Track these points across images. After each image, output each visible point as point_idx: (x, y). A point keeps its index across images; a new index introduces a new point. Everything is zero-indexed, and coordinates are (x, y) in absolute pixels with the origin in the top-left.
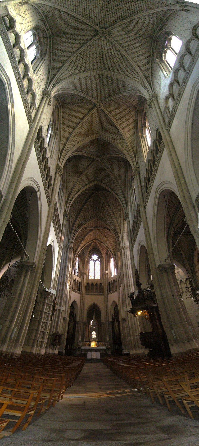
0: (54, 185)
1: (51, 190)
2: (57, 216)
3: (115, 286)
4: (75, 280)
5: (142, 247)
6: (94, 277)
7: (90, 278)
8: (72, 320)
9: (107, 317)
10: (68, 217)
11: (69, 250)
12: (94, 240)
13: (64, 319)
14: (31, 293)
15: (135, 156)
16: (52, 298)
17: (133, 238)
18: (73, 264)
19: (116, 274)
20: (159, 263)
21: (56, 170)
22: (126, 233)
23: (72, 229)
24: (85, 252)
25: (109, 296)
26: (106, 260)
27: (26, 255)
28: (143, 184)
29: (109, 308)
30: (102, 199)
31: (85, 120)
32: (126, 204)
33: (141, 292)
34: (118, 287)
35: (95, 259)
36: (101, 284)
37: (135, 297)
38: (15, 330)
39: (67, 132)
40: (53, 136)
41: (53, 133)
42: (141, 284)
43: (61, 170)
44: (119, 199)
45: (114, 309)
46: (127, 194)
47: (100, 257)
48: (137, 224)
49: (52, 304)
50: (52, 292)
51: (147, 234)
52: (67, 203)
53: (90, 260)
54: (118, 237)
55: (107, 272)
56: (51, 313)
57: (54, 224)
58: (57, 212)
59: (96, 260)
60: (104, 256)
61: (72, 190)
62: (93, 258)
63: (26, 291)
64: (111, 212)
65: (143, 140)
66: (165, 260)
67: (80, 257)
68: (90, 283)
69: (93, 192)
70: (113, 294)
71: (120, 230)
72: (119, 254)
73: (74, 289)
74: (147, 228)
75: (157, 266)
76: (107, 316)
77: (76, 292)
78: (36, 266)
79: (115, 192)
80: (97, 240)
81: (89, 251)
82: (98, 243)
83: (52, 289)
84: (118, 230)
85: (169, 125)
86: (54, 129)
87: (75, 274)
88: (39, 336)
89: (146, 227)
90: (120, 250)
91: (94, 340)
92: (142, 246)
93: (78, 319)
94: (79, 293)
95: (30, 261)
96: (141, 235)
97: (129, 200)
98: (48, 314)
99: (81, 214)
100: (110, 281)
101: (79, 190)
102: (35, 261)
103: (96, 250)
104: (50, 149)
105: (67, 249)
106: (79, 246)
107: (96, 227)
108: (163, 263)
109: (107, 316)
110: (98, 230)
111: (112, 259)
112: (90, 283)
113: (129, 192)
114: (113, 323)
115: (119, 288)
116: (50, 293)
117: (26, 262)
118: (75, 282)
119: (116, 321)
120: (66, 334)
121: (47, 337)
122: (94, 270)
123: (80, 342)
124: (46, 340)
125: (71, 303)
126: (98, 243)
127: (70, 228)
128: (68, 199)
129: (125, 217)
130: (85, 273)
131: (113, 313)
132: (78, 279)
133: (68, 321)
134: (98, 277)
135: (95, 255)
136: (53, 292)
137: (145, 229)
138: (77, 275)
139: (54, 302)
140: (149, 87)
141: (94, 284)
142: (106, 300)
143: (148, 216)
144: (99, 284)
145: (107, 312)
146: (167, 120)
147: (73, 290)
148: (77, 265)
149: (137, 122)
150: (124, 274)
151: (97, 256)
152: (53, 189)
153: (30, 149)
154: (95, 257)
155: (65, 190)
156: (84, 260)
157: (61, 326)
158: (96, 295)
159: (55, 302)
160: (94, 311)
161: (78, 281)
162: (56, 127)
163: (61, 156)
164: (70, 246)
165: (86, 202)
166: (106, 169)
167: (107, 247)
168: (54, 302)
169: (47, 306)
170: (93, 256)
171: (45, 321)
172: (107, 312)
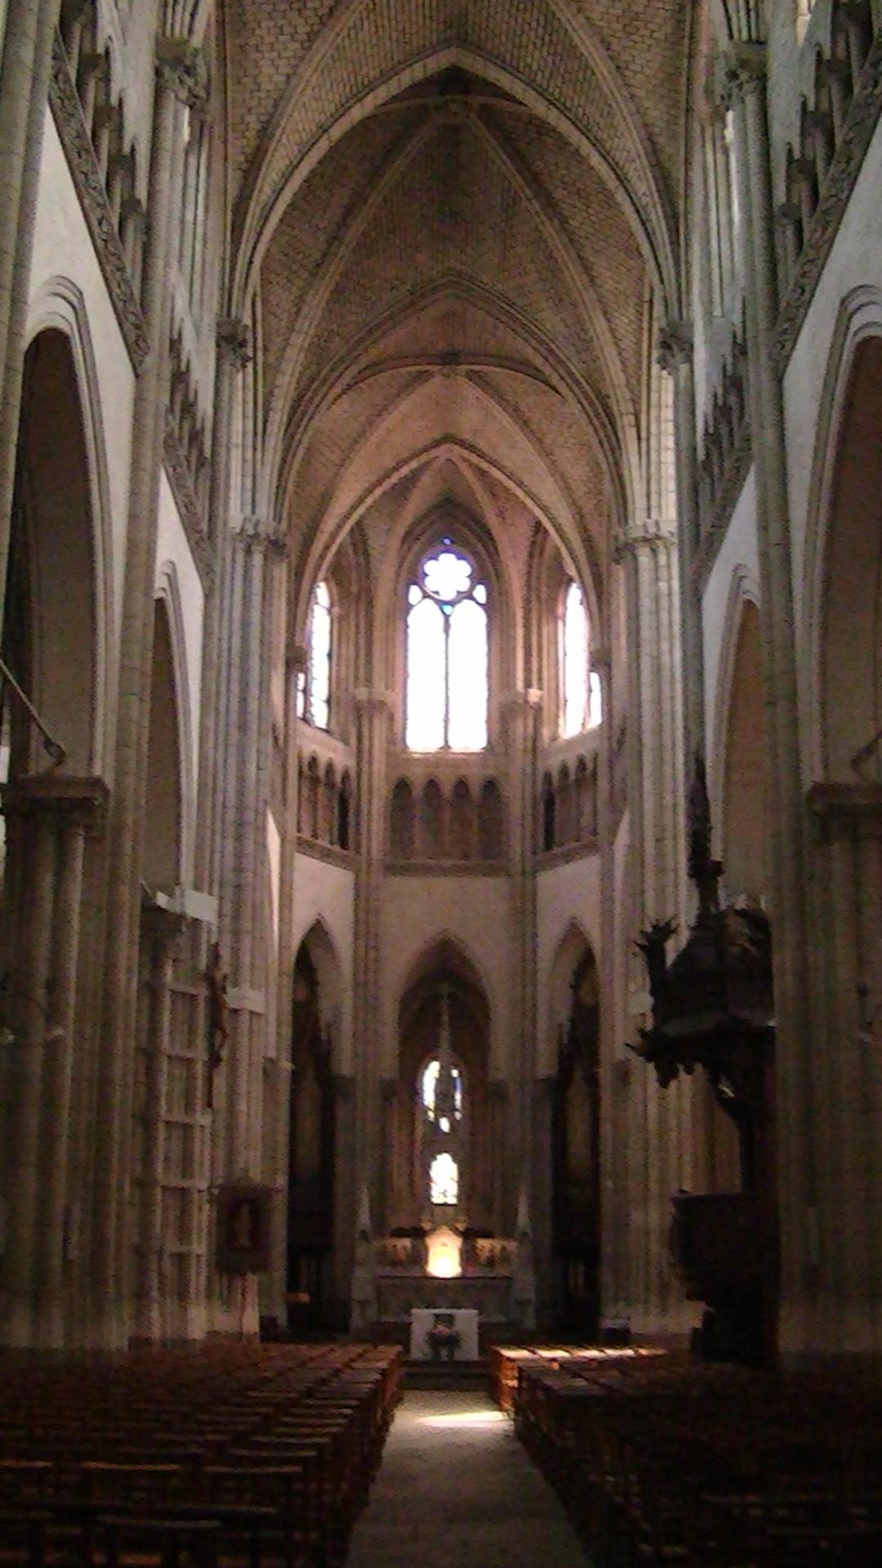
0: (151, 196)
1: (208, 484)
2: (96, 64)
3: (587, 808)
4: (314, 761)
8: (311, 1075)
9: (525, 1042)
12: (437, 444)
13: (269, 1071)
14: (109, 967)
16: (195, 949)
17: (789, 269)
18: (290, 645)
19: (596, 720)
20: (818, 775)
21: (158, 72)
22: (669, 414)
24: (375, 542)
25: (546, 879)
26: (527, 601)
27: (48, 743)
28: (780, 195)
29: (542, 977)
30: (500, 160)
32: (675, 243)
33: (709, 923)
36: (490, 786)
37: (673, 949)
38: (76, 1217)
42: (718, 869)
43: (189, 71)
44: (620, 196)
45: (575, 987)
46: (688, 162)
47: (487, 572)
49: (203, 992)
50: (192, 911)
52: (236, 242)
53: (415, 593)
54: (614, 449)
55: (534, 695)
56: (200, 1054)
57: (177, 485)
60: (515, 571)
61: (265, 132)
62: (430, 584)
64: (564, 255)
65: (720, 158)
66: (855, 763)
67: (337, 577)
69: (425, 108)
70: (567, 870)
71: (635, 402)
72: (621, 573)
73: (306, 835)
74: (774, 513)
75: (807, 786)
76: (524, 1029)
77: (325, 855)
78: (106, 791)
79: (596, 143)
80: (462, 443)
81: (401, 529)
82: (468, 473)
83: (190, 893)
84: (621, 404)
87: (306, 719)
88: (164, 1226)
89: (773, 505)
90: (624, 551)
91: (443, 1216)
93: (345, 1064)
94: (343, 863)
95: (74, 768)
96: (741, 540)
97: (697, 215)
98: (189, 1062)
100: (554, 764)
101: (324, 130)
102: (97, 771)
103: (457, 522)
105: (248, 552)
106: (326, 499)
107: (450, 359)
108: (844, 775)
110: (473, 376)
111: (575, 594)
113: (697, 159)
114: (559, 1086)
115: (613, 830)
116: (182, 917)
117: (47, 779)
118: (315, 780)
119: (578, 1075)
121: (203, 1216)
122: (445, 690)
123: (364, 1236)
124: (200, 1247)
125: (295, 943)
126: (468, 473)
130: (376, 707)
131: (564, 1015)
132: (335, 754)
133: (284, 1086)
134: (471, 736)
135: (447, 559)
136: (200, 906)
137: (763, 527)
139: (210, 979)
140: (671, 262)
141: (447, 790)
142: (525, 909)
143: (790, 426)
144: (476, 790)
145: (526, 1008)
146: (705, 529)
147: (305, 847)
150: (648, 739)
152: (148, 230)
153: (154, 495)
155: (217, 143)
156: (370, 604)
157: (257, 1124)
158: (460, 871)
159: (219, 976)
160: (444, 1006)
163: (267, 411)
165: (375, 174)
168: (210, 979)
170: (430, 567)
171: (178, 1116)
172: (526, 1008)
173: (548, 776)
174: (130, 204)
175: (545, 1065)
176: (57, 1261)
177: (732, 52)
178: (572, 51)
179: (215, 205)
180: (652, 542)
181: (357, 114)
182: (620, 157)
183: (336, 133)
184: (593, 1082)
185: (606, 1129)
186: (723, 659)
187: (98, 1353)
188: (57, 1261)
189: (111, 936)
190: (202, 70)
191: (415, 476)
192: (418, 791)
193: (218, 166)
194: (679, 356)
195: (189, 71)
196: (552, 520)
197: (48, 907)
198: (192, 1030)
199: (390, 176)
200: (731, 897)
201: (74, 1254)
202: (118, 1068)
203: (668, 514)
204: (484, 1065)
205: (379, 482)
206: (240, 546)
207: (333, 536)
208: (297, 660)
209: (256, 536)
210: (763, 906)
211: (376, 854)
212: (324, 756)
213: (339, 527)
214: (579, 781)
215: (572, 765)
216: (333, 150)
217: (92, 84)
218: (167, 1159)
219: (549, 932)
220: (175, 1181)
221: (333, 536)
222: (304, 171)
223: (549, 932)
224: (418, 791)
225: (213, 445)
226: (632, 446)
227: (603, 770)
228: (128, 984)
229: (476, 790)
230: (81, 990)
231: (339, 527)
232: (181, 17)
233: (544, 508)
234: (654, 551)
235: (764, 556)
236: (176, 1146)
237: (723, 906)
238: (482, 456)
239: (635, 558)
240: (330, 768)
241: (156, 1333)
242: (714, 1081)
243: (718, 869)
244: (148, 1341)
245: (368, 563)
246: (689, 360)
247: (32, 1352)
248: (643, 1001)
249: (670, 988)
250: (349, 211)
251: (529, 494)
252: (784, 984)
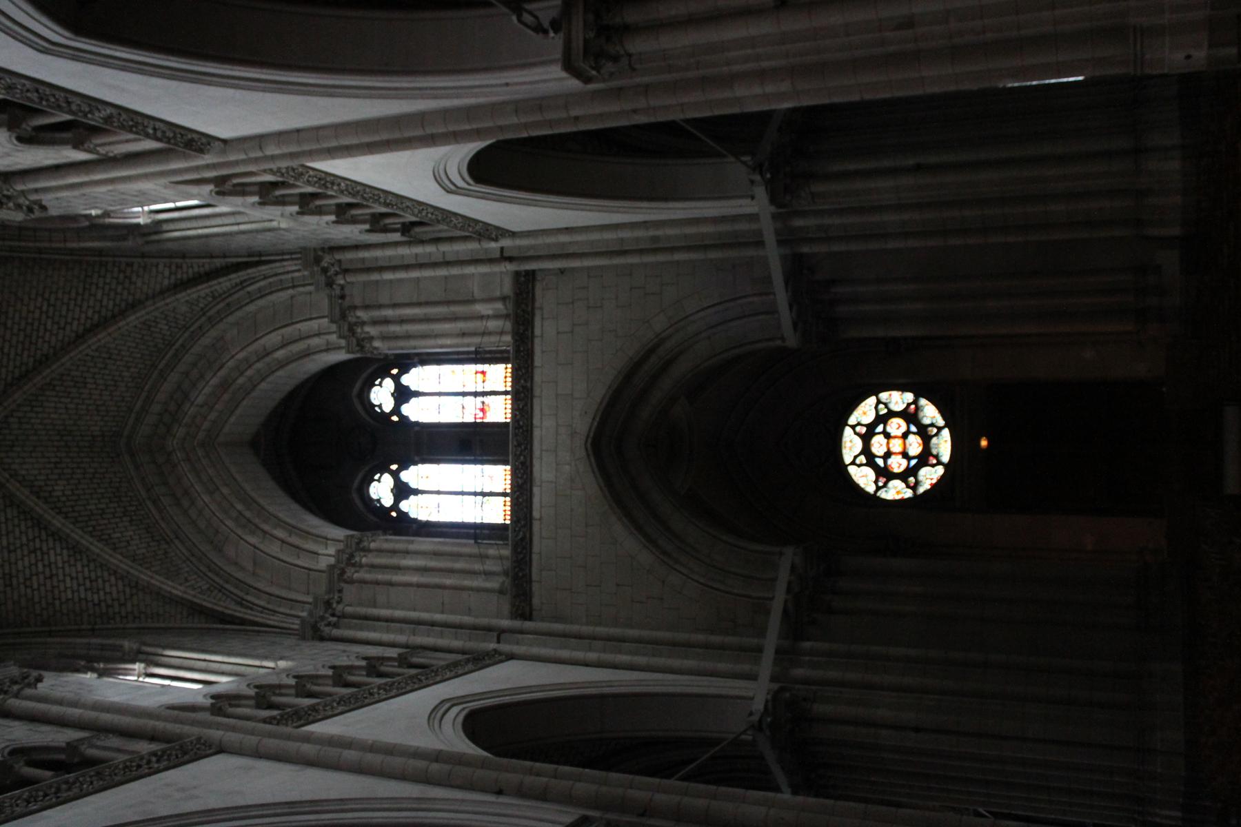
65: (165, 227)
75: (574, 84)
85: (189, 142)
153: (332, 742)
186: (601, 210)
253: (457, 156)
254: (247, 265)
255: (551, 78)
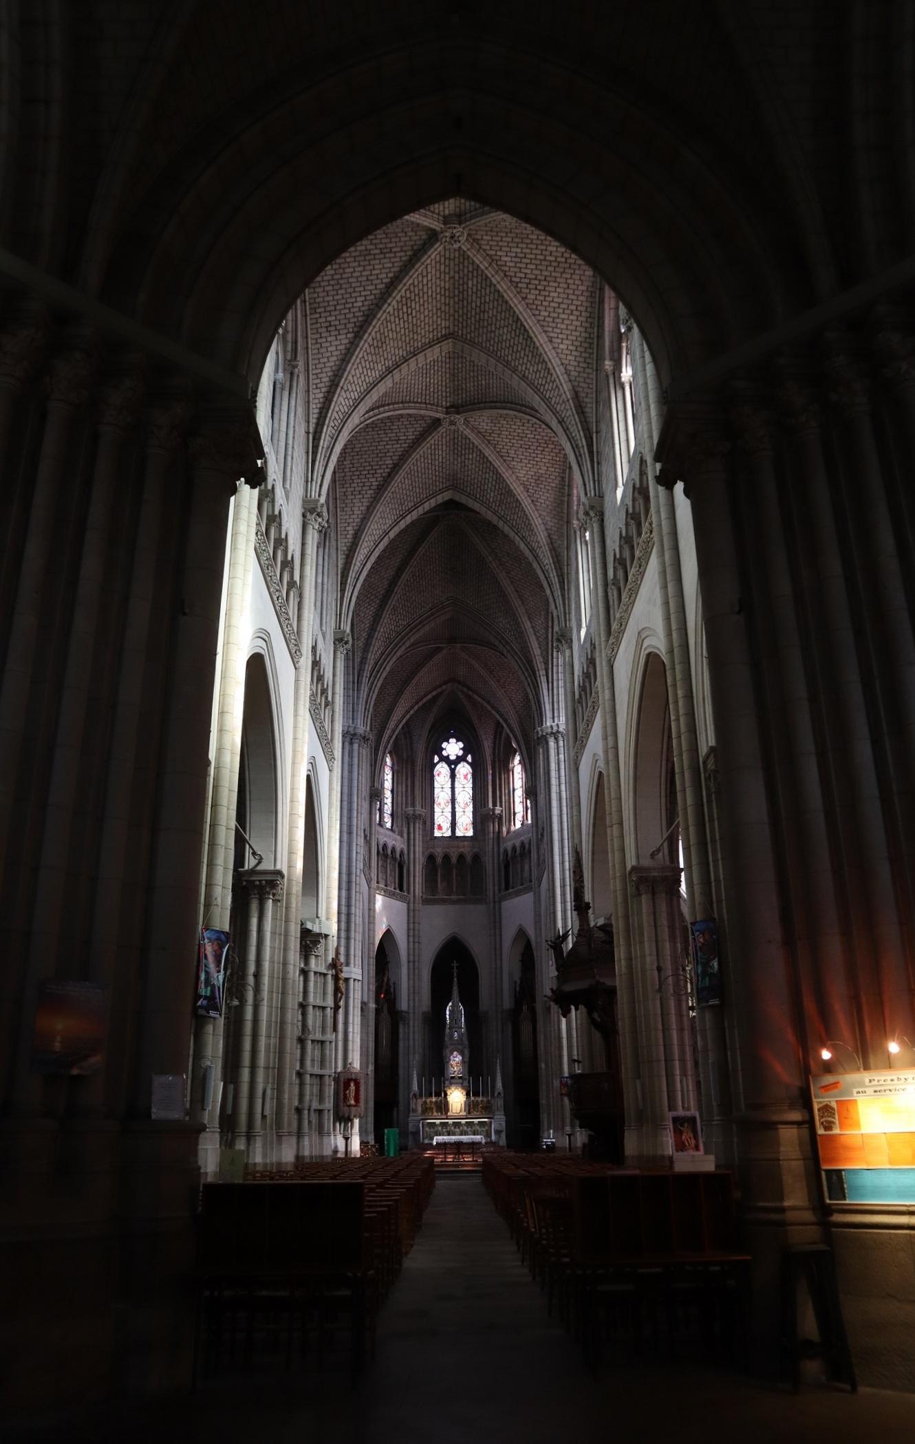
1: (297, 600)
4: (385, 846)
5: (652, 659)
6: (453, 830)
7: (437, 834)
10: (325, 514)
11: (356, 746)
12: (445, 683)
14: (285, 964)
15: (590, 446)
16: (326, 950)
17: (581, 727)
20: (634, 863)
21: (304, 516)
23: (361, 670)
25: (505, 904)
27: (254, 854)
29: (505, 957)
31: (398, 295)
32: (562, 589)
33: (585, 931)
34: (535, 873)
35: (453, 757)
36: (477, 858)
38: (269, 1092)
39: (334, 346)
40: (282, 389)
41: (280, 375)
42: (588, 906)
46: (568, 548)
48: (637, 553)
51: (611, 757)
52: (343, 591)
53: (436, 759)
54: (536, 687)
55: (498, 810)
56: (330, 1002)
58: (273, 501)
59: (460, 759)
62: (444, 753)
63: (272, 961)
66: (653, 855)
67: (396, 753)
68: (439, 852)
69: (438, 420)
71: (546, 663)
74: (611, 731)
75: (629, 867)
76: (497, 979)
78: (283, 877)
79: (523, 538)
80: (459, 682)
81: (428, 726)
82: (461, 696)
84: (540, 666)
86: (285, 352)
87: (381, 824)
88: (312, 1094)
89: (609, 729)
92: (649, 655)
93: (403, 1005)
94: (402, 899)
95: (266, 866)
96: (595, 741)
99: (393, 602)
100: (509, 845)
102: (278, 867)
104: (277, 453)
105: (351, 743)
108: (647, 862)
109: (497, 979)
111: (517, 758)
112: (439, 852)
114: (514, 1016)
117: (253, 872)
119: (525, 1008)
120: (371, 1068)
126: (461, 696)
127: (357, 660)
128: (343, 584)
129: (559, 640)
131: (517, 977)
132: (396, 842)
133: (372, 1016)
134: (465, 827)
135: (453, 740)
137: (605, 738)
138: (389, 825)
141: (454, 860)
142: (496, 922)
144: (469, 859)
148: (388, 784)
149: (602, 302)
151: (461, 745)
152: (301, 596)
154: (453, 748)
155: (334, 543)
161: (393, 849)
162: (289, 337)
164: (361, 729)
166: (487, 452)
167: (498, 712)
169: (316, 982)
170: (444, 745)
173: (506, 851)
174: (291, 584)
175: (508, 1003)
176: (258, 1116)
177: (587, 503)
178: (510, 493)
179: (333, 572)
180: (555, 735)
181: (402, 525)
182: (535, 545)
183: (392, 535)
184: (533, 1011)
185: (541, 1037)
186: (590, 792)
187: (279, 1164)
188: (258, 1116)
189: (286, 949)
190: (325, 514)
191: (435, 699)
192: (439, 860)
193: (333, 552)
194: (565, 646)
195: (319, 515)
196: (505, 720)
197: (254, 934)
198: (325, 993)
199: (421, 551)
200: (596, 920)
201: (267, 1112)
202: (289, 1016)
203: (562, 722)
204: (477, 1002)
205: (417, 703)
206: (348, 739)
207: (394, 731)
208: (375, 795)
209: (355, 734)
210: (420, 1259)
211: (418, 892)
212: (390, 843)
213: (397, 726)
214: (522, 855)
215: (518, 845)
216: (392, 542)
217: (265, 504)
218: (313, 1060)
219: (509, 933)
220: (317, 1071)
221: (394, 731)
222: (376, 553)
223: (509, 933)
224: (439, 860)
225: (333, 694)
226: (544, 686)
227: (534, 849)
228: (294, 973)
229: (469, 859)
230: (271, 977)
231: (397, 726)
232: (315, 487)
233: (501, 716)
234: (556, 739)
235: (606, 752)
236: (317, 1053)
237: (592, 924)
238: (469, 689)
239: (547, 743)
240: (393, 849)
241: (307, 1153)
242: (590, 1013)
243: (588, 906)
244: (303, 1157)
245: (411, 744)
246: (571, 648)
247: (265, 1165)
248: (553, 973)
249: (566, 965)
250: (398, 575)
251: (493, 707)
252: (620, 965)
253: (658, 643)
254: (591, 452)
255: (631, 862)
